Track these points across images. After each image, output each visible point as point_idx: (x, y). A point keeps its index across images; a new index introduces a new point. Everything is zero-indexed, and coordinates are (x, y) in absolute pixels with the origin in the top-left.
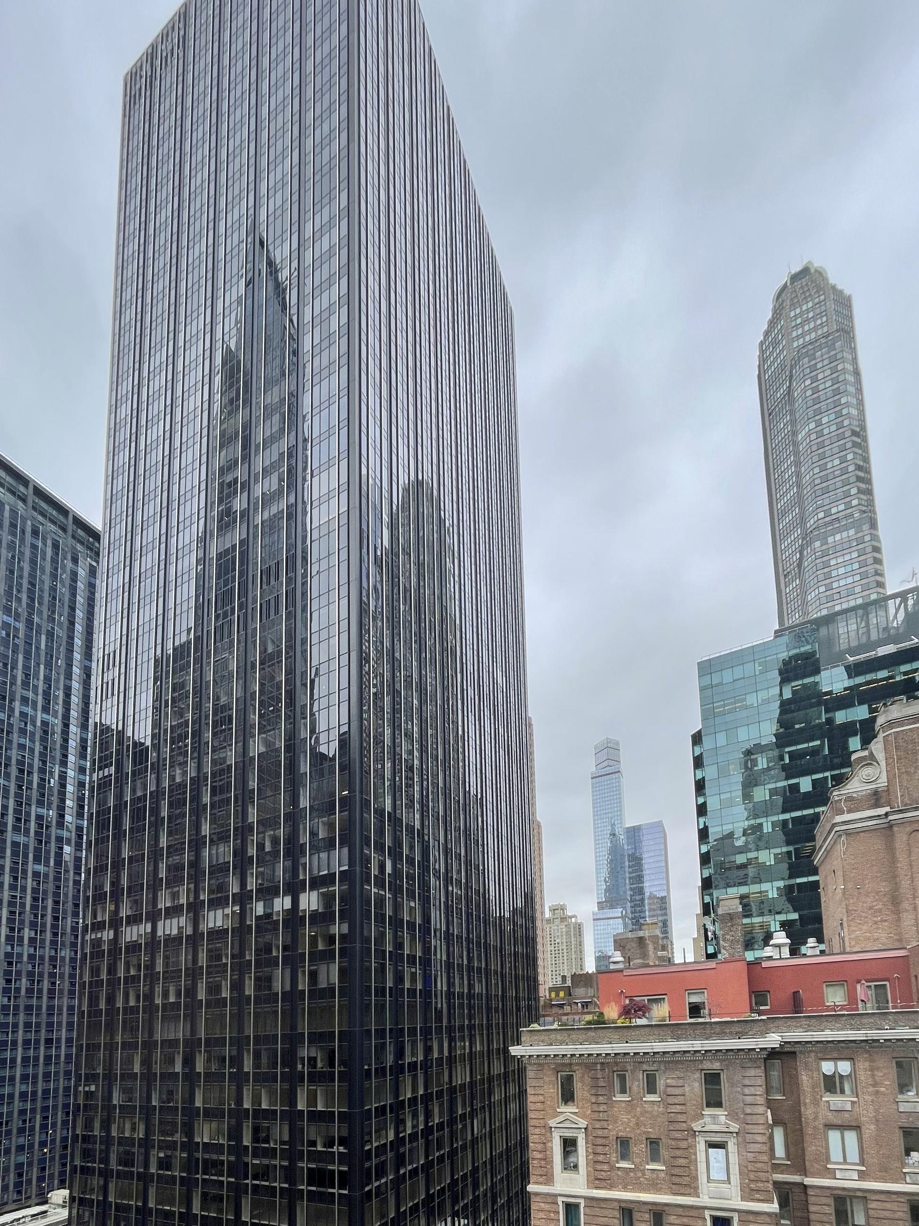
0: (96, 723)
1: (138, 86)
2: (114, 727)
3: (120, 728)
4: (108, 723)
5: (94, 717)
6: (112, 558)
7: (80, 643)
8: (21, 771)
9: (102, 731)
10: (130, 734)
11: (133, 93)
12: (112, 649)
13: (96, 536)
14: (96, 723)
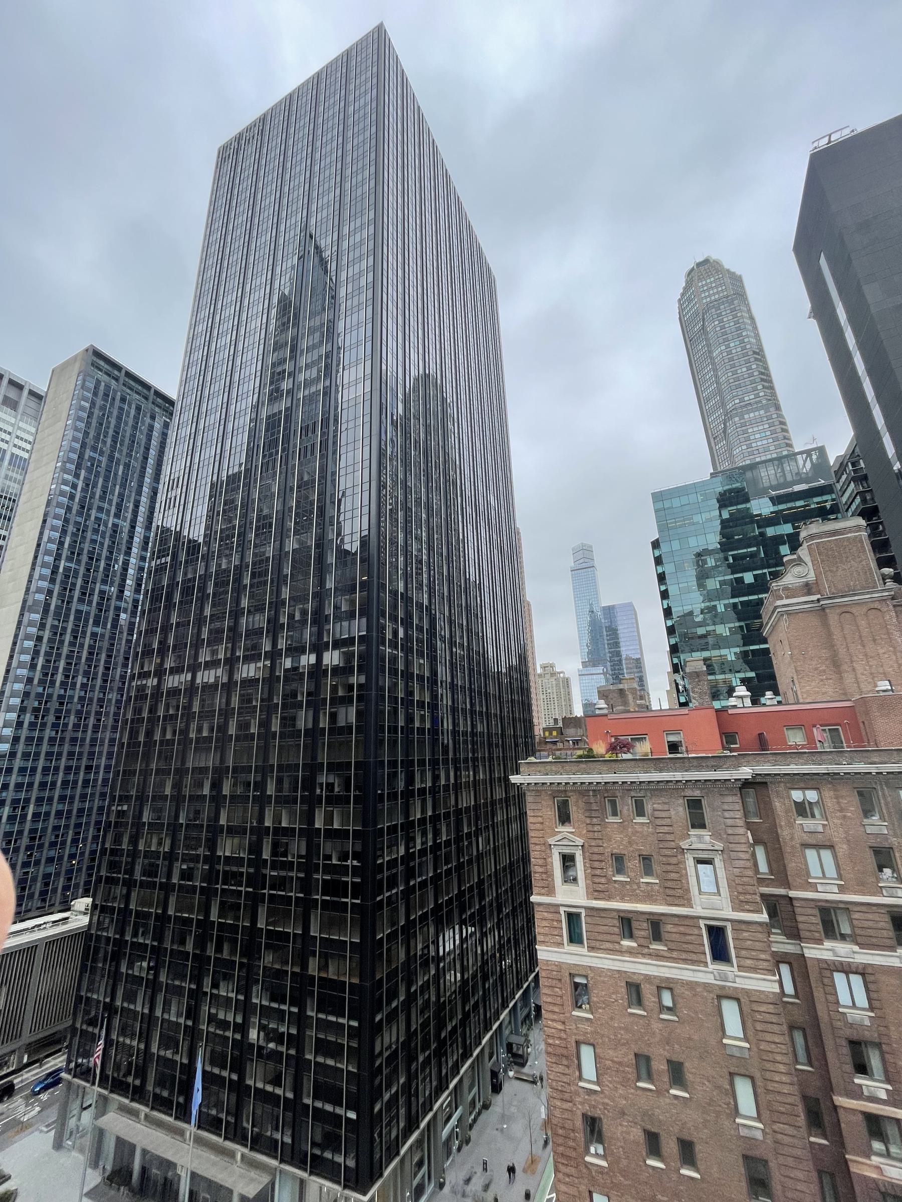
0: (158, 526)
2: (173, 529)
3: (178, 529)
4: (169, 526)
5: (157, 521)
6: (181, 429)
7: (151, 471)
8: (91, 559)
9: (162, 532)
10: (186, 534)
12: (177, 476)
13: (172, 403)
14: (158, 526)
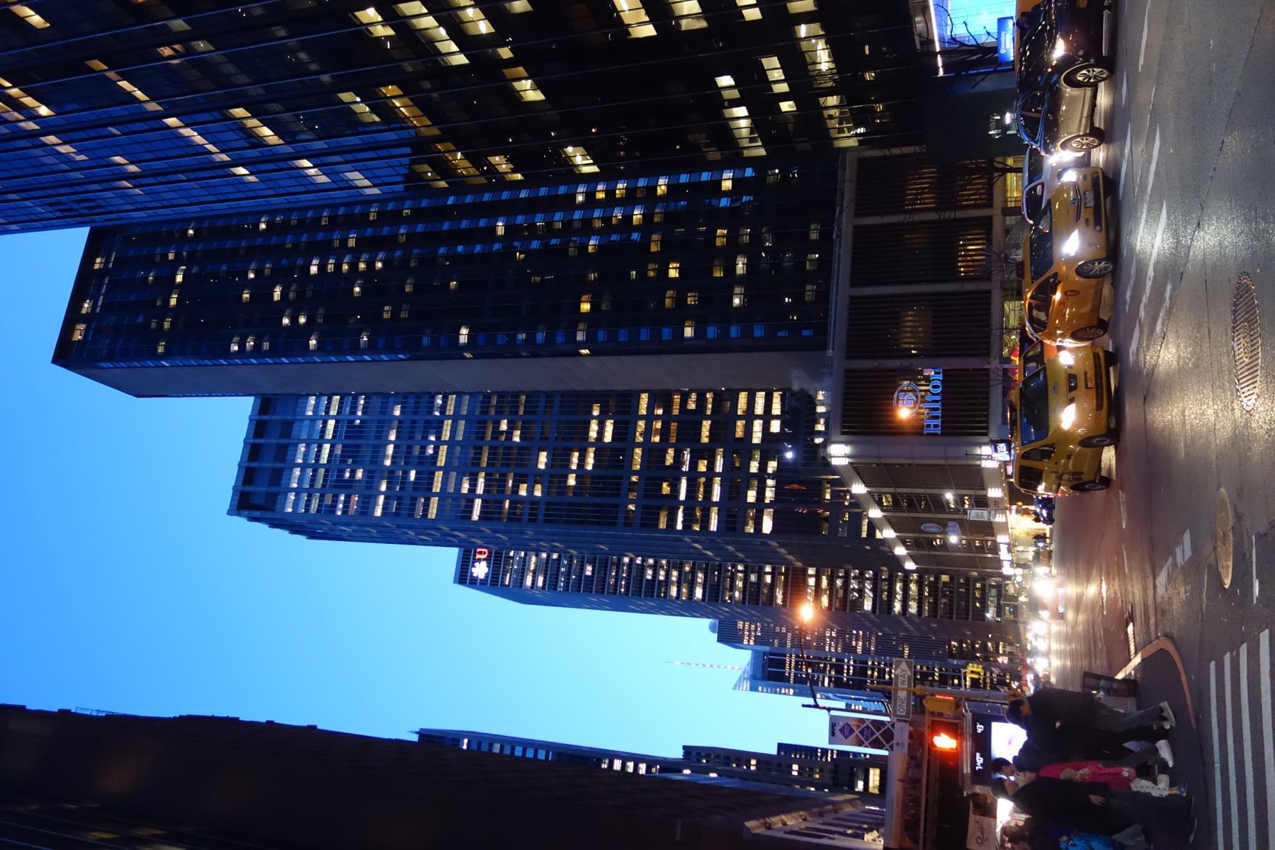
1: (75, 206)
3: (407, 150)
11: (59, 214)
